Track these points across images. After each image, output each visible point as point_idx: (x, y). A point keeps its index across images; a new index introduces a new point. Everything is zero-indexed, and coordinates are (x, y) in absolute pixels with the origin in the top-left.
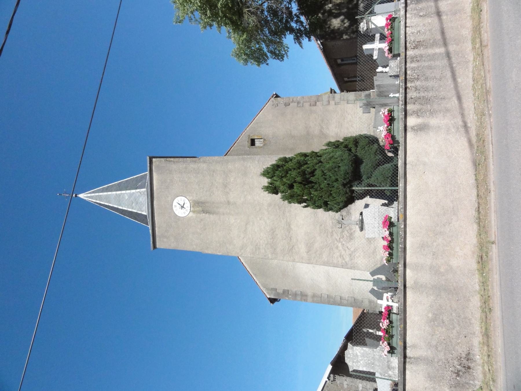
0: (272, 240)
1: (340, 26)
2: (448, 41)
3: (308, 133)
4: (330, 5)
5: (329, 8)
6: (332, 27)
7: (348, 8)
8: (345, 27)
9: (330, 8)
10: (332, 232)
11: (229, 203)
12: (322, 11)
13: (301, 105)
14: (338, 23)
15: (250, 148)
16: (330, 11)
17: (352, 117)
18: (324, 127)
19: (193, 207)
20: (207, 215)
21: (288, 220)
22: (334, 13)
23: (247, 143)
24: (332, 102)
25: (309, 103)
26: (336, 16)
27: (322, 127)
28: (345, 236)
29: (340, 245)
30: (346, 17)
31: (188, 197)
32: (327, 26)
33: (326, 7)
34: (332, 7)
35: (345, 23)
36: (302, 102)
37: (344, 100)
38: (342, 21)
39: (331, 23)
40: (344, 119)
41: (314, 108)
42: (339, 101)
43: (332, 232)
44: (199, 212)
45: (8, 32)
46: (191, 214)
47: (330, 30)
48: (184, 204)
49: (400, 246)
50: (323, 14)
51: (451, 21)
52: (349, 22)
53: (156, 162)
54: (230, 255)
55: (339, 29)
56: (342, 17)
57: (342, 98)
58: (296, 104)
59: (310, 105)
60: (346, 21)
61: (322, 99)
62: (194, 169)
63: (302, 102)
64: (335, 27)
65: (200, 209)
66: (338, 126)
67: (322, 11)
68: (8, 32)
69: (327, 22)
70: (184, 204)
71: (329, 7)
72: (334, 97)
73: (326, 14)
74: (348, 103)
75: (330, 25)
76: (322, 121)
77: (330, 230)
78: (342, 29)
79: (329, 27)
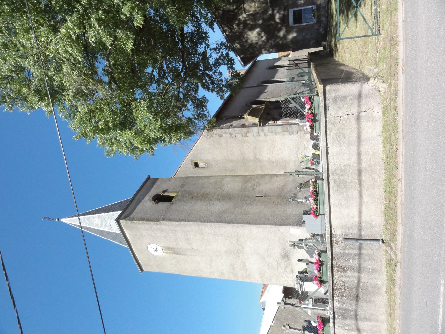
0: (232, 271)
1: (258, 40)
2: (357, 173)
3: (244, 159)
4: (245, 15)
5: (243, 19)
6: (249, 41)
7: (263, 20)
8: (263, 41)
9: (245, 18)
10: (278, 268)
11: (193, 249)
12: (236, 22)
13: (234, 135)
14: (256, 37)
15: (195, 169)
16: (245, 22)
17: (281, 146)
18: (257, 153)
19: (165, 250)
20: (178, 255)
21: (243, 261)
22: (249, 24)
23: (191, 165)
24: (262, 134)
25: (241, 135)
26: (252, 29)
27: (255, 154)
28: (288, 271)
29: (284, 275)
30: (263, 30)
31: (159, 245)
32: (244, 40)
33: (241, 17)
34: (247, 17)
35: (262, 37)
36: (234, 134)
37: (272, 132)
38: (259, 34)
39: (249, 36)
40: (274, 147)
41: (246, 139)
42: (268, 133)
43: (278, 268)
44: (171, 253)
45: (14, 305)
46: (165, 254)
47: (248, 44)
48: (157, 248)
49: (329, 264)
50: (238, 25)
51: (366, 49)
52: (266, 35)
53: (123, 223)
54: (202, 276)
55: (257, 43)
56: (258, 30)
57: (271, 130)
58: (229, 135)
59: (242, 136)
60: (263, 34)
61: (252, 131)
62: (158, 229)
63: (234, 134)
64: (252, 40)
65: (171, 251)
66: (269, 153)
67: (236, 22)
68: (14, 305)
69: (244, 35)
70: (157, 248)
71: (243, 17)
72: (263, 130)
73: (241, 26)
74: (276, 135)
75: (248, 38)
76: (255, 149)
77: (276, 268)
78: (261, 43)
79: (246, 41)
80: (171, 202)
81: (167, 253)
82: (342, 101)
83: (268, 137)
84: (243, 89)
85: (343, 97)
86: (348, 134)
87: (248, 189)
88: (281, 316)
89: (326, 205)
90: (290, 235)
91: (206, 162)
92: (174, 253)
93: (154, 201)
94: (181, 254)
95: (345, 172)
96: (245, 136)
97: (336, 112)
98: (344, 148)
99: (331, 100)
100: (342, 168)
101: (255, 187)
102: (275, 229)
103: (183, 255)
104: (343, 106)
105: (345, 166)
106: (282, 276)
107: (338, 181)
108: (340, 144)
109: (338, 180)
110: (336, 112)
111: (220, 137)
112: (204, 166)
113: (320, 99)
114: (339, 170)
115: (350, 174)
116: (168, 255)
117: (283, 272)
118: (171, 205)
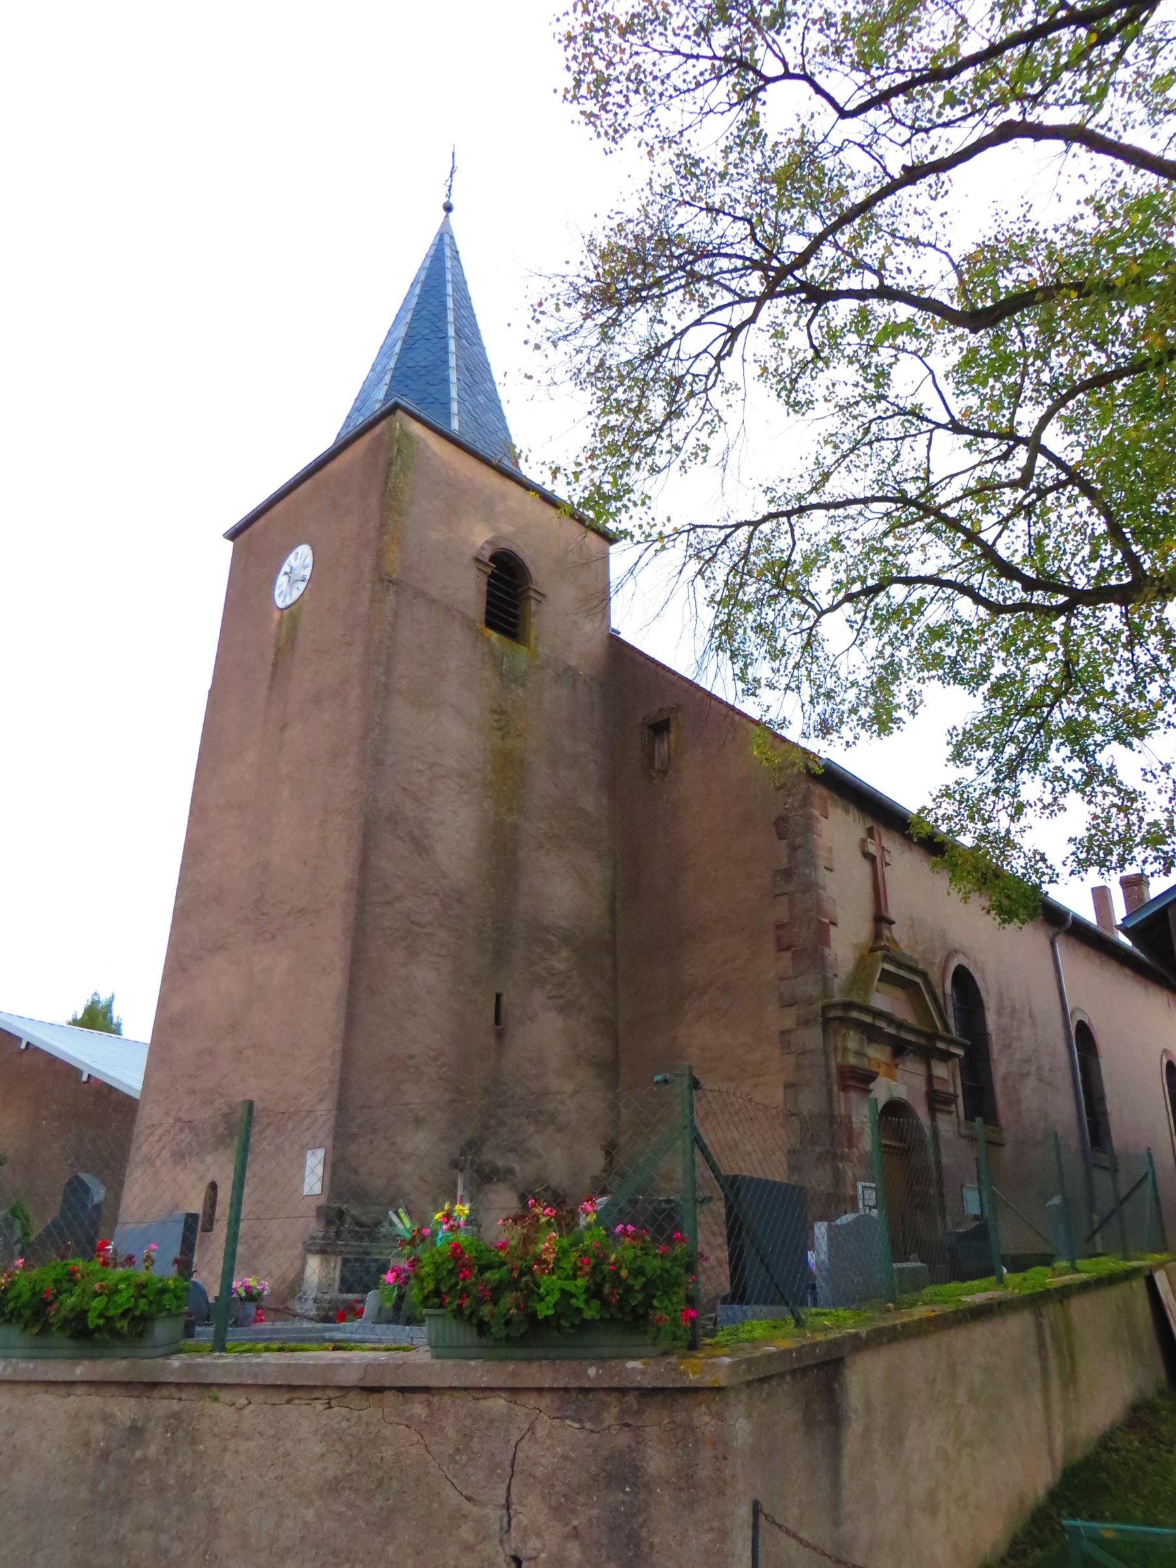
10: (195, 1092)
24: (789, 1020)
25: (786, 920)
36: (790, 888)
37: (799, 1067)
41: (769, 946)
43: (195, 1092)
46: (276, 615)
58: (784, 864)
59: (780, 926)
63: (790, 888)
74: (785, 1087)
80: (483, 626)
81: (280, 623)
82: (612, 1529)
83: (777, 1051)
84: (1047, 943)
85: (634, 1539)
86: (390, 1550)
87: (542, 959)
88: (110, 1111)
89: (23, 1365)
90: (304, 1148)
91: (671, 773)
92: (279, 651)
93: (493, 558)
94: (272, 680)
95: (176, 1511)
96: (778, 939)
97: (539, 1471)
98: (310, 1515)
99: (623, 1439)
100: (199, 1492)
101: (549, 987)
102: (326, 1080)
103: (270, 688)
104: (575, 1534)
105: (212, 1511)
106: (167, 1114)
107: (133, 1452)
108: (333, 1488)
109: (138, 1454)
110: (539, 1471)
111: (776, 824)
112: (657, 766)
113: (631, 1364)
114: (188, 1468)
115: (164, 1539)
116: (273, 627)
117: (181, 1115)
118: (467, 623)
